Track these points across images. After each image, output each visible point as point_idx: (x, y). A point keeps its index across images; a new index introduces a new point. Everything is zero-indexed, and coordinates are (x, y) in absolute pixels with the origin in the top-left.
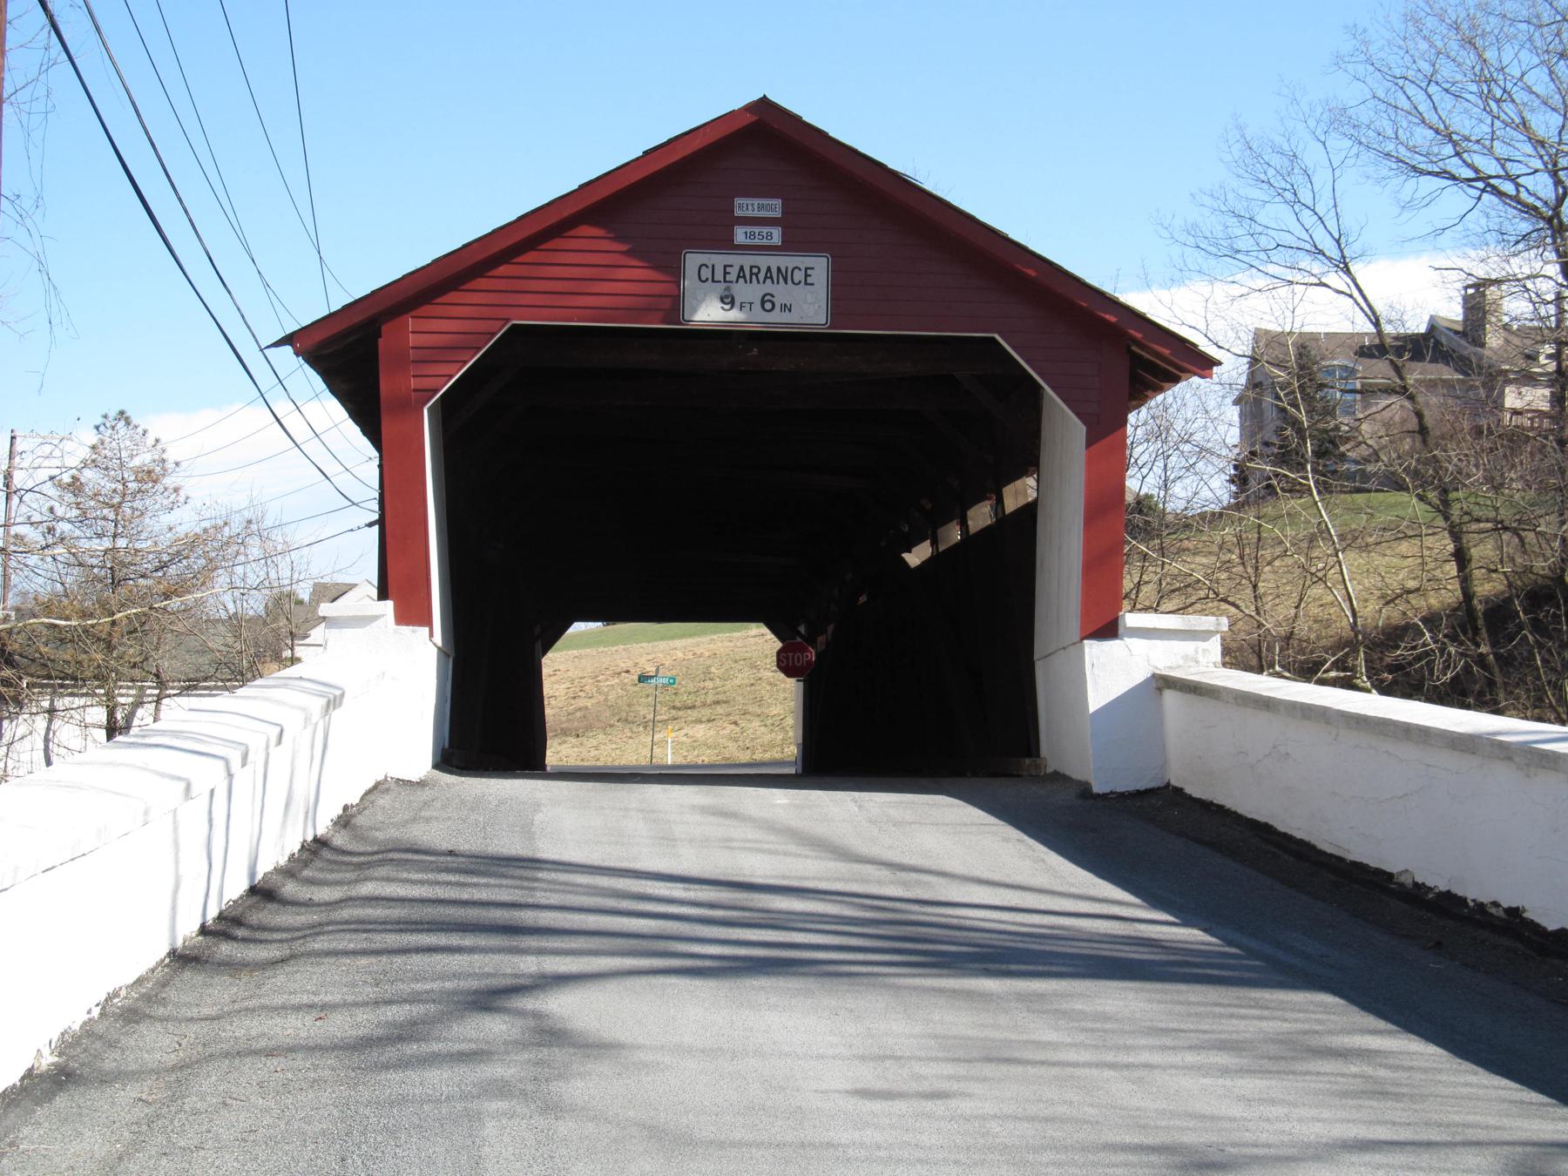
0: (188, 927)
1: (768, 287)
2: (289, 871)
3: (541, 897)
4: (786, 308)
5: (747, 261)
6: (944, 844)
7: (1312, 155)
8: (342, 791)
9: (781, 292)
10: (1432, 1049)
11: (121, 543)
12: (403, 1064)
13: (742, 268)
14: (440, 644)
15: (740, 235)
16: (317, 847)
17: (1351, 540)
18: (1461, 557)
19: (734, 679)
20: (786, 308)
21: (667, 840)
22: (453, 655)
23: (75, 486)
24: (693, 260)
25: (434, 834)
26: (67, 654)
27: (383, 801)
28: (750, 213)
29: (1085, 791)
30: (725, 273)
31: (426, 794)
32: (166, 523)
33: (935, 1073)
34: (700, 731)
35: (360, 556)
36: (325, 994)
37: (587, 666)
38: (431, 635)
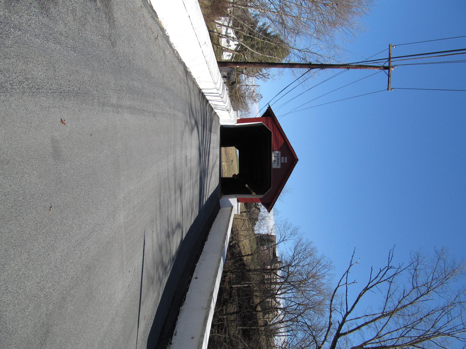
0: (204, 91)
2: (210, 105)
3: (207, 131)
5: (280, 159)
6: (213, 183)
7: (296, 237)
8: (219, 112)
9: (276, 162)
10: (193, 222)
12: (189, 110)
15: (283, 158)
16: (212, 109)
17: (250, 240)
18: (248, 255)
19: (232, 169)
21: (214, 148)
23: (254, 92)
25: (214, 123)
27: (217, 118)
29: (220, 199)
32: (249, 102)
33: (189, 165)
34: (226, 168)
36: (196, 103)
37: (233, 152)
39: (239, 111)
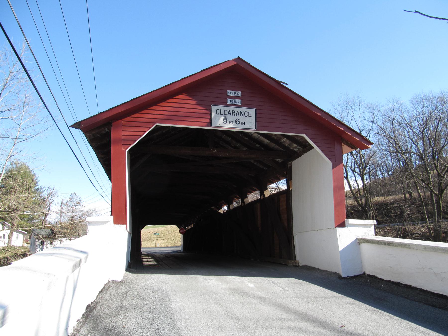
1: (238, 117)
4: (243, 123)
5: (231, 109)
9: (242, 119)
11: (73, 214)
13: (229, 111)
14: (129, 231)
15: (229, 101)
20: (243, 123)
22: (131, 233)
24: (214, 108)
26: (64, 231)
28: (231, 95)
30: (224, 112)
31: (123, 289)
34: (162, 241)
35: (105, 205)
38: (126, 228)
39: (88, 219)
